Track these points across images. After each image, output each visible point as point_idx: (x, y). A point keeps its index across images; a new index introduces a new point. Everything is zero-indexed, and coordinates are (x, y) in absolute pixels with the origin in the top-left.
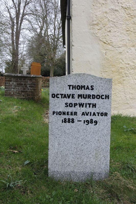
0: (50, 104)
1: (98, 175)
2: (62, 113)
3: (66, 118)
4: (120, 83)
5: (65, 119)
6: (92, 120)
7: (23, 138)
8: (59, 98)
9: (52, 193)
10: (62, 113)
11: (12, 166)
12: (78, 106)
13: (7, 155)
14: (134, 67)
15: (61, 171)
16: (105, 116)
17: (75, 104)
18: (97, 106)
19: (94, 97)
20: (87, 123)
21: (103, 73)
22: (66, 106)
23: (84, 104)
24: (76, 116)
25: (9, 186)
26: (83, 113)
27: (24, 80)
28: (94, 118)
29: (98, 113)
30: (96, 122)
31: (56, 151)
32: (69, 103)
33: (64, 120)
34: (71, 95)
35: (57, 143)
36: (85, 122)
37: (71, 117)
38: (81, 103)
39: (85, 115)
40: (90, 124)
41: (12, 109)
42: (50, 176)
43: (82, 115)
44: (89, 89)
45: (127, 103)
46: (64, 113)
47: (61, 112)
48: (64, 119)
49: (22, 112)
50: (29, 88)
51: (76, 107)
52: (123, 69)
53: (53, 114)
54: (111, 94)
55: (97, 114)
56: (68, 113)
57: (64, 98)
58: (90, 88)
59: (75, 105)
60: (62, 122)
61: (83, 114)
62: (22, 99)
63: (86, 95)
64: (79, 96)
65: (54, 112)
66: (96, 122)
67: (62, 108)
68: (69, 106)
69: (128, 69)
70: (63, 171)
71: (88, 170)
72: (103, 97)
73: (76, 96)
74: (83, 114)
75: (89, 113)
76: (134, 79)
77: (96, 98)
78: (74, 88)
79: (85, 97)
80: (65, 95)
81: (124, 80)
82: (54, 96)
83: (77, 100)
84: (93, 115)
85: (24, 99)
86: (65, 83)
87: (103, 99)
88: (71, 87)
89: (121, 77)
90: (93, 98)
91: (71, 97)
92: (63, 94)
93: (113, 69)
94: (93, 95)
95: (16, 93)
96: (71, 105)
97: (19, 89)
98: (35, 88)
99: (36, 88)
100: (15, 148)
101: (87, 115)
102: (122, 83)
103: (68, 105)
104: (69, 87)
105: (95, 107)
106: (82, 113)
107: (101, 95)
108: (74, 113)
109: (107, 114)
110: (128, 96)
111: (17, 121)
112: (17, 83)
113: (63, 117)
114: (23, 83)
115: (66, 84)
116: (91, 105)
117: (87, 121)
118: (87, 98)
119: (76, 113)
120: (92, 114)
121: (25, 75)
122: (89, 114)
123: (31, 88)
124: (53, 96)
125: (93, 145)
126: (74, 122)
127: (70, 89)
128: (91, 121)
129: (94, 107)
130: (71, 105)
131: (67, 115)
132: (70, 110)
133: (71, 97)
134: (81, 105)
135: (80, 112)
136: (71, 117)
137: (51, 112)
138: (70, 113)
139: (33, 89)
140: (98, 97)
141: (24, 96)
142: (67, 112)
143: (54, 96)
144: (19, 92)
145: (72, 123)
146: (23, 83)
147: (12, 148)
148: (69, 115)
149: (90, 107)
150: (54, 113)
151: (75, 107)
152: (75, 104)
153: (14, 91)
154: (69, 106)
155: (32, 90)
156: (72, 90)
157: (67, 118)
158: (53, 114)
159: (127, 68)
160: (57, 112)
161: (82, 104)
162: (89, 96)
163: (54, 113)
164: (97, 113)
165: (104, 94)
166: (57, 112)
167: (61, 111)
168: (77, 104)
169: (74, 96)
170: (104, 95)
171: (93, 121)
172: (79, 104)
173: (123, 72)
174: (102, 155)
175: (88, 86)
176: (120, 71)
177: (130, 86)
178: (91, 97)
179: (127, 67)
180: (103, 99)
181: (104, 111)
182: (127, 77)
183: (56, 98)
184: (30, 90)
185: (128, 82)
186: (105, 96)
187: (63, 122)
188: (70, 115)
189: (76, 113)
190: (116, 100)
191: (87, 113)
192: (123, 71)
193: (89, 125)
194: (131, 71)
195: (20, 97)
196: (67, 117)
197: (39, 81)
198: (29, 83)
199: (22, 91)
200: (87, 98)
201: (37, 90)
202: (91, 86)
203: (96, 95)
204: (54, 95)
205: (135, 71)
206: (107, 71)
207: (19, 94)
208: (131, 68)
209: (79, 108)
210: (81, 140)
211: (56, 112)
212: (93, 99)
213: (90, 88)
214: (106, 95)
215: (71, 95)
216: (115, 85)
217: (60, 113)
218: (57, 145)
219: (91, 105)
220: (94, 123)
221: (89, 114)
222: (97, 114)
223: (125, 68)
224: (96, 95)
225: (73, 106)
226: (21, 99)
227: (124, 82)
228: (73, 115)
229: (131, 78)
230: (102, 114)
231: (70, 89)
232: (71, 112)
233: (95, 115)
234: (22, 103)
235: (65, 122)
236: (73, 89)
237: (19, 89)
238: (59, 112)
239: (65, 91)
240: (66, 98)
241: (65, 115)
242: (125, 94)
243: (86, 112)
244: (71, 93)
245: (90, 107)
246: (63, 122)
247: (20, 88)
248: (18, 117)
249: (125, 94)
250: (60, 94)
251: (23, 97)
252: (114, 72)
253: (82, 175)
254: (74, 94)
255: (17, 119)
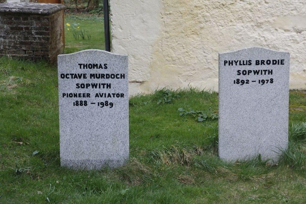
0: (59, 85)
1: (117, 162)
2: (73, 95)
3: (78, 100)
4: (195, 33)
5: (77, 102)
6: (107, 102)
7: (29, 128)
8: (69, 78)
9: (63, 179)
10: (73, 95)
11: (18, 158)
12: (91, 86)
13: (10, 147)
14: (219, 4)
15: (74, 159)
16: (121, 97)
17: (87, 84)
18: (112, 86)
19: (108, 77)
20: (102, 106)
21: (165, 17)
22: (77, 88)
23: (97, 84)
24: (89, 98)
25: (18, 171)
26: (97, 94)
27: (25, 20)
28: (110, 100)
29: (114, 94)
30: (111, 104)
31: (69, 138)
32: (80, 84)
33: (75, 103)
34: (83, 75)
35: (69, 129)
36: (100, 104)
37: (83, 99)
38: (94, 84)
39: (98, 97)
40: (105, 107)
41: (5, 82)
42: (62, 165)
43: (96, 97)
44: (102, 68)
45: (209, 68)
46: (75, 95)
47: (72, 94)
48: (237, 80)
49: (25, 89)
50: (36, 36)
51: (88, 87)
52: (199, 8)
53: (63, 97)
54: (127, 73)
55: (112, 96)
56: (80, 95)
57: (74, 78)
58: (103, 67)
59: (88, 85)
60: (74, 105)
61: (97, 95)
62: (22, 60)
63: (99, 75)
64: (92, 76)
65: (103, 74)
66: (112, 105)
67: (73, 90)
68: (80, 87)
69: (209, 8)
70: (77, 159)
71: (104, 158)
72: (118, 76)
73: (88, 76)
74: (97, 95)
75: (104, 94)
76: (220, 25)
77: (110, 78)
78: (85, 67)
79: (98, 76)
80: (76, 74)
81: (202, 28)
82: (63, 76)
83: (89, 80)
84: (108, 97)
85: (26, 58)
86: (75, 62)
87: (119, 78)
88: (82, 66)
89: (197, 23)
90: (107, 78)
91: (82, 77)
92: (73, 74)
93: (182, 9)
94: (107, 75)
95: (9, 46)
96: (82, 86)
97: (15, 38)
98: (48, 36)
99: (49, 37)
100: (20, 140)
101: (101, 96)
102: (198, 33)
103: (80, 85)
104: (79, 66)
105: (110, 88)
106: (95, 95)
107: (115, 74)
108: (86, 94)
109: (123, 94)
110: (209, 56)
111: (17, 103)
112: (10, 26)
113: (75, 99)
114: (23, 26)
115: (76, 63)
116: (106, 86)
117: (102, 104)
118: (101, 77)
119: (88, 95)
120: (107, 95)
121: (26, 11)
122: (104, 95)
123: (39, 36)
124: (63, 76)
125: (110, 130)
126: (86, 105)
127: (81, 68)
128: (106, 103)
129: (109, 87)
130: (82, 86)
131: (79, 97)
132: (82, 91)
133: (82, 77)
134: (95, 86)
135: (94, 94)
136: (83, 99)
137: (60, 95)
138: (82, 95)
139: (44, 38)
140: (113, 76)
141: (25, 53)
142: (79, 94)
143: (63, 76)
144: (16, 44)
145: (85, 106)
146: (23, 26)
147: (16, 140)
148: (81, 97)
149: (104, 87)
150: (64, 95)
151: (87, 88)
152: (87, 84)
153: (5, 42)
154: (80, 87)
155: (43, 40)
156: (83, 69)
157: (242, 70)
158: (63, 97)
159: (207, 7)
160: (67, 94)
161: (96, 84)
162: (103, 76)
163: (64, 95)
164: (112, 94)
165: (119, 73)
166: (67, 94)
167: (72, 93)
168: (89, 85)
169: (86, 76)
170: (119, 75)
171: (109, 103)
172: (92, 84)
173: (200, 14)
174: (120, 141)
175: (101, 65)
176: (195, 12)
177: (213, 39)
178: (105, 77)
179: (206, 6)
180: (119, 78)
181: (120, 92)
182: (207, 23)
183: (65, 78)
184: (37, 40)
185: (210, 31)
186: (120, 75)
187: (75, 105)
188: (82, 97)
189: (88, 95)
190: (190, 64)
191: (101, 94)
192: (199, 12)
193: (104, 107)
194: (213, 12)
195: (19, 54)
196: (79, 99)
197: (57, 19)
198: (35, 25)
199: (21, 43)
200: (101, 77)
201: (52, 38)
202: (105, 65)
203: (110, 75)
204: (64, 75)
205: (221, 11)
206: (171, 12)
207: (16, 49)
208: (214, 6)
209: (92, 89)
210: (96, 124)
211: (66, 94)
212: (107, 79)
213: (103, 67)
214: (121, 74)
215: (83, 75)
216: (186, 37)
217: (71, 95)
218: (68, 131)
219: (106, 86)
220: (109, 106)
221: (104, 95)
222: (112, 96)
223: (204, 7)
224: (110, 75)
225: (85, 87)
226: (21, 58)
227: (202, 31)
228: (85, 97)
229: (214, 23)
230: (118, 96)
231: (81, 68)
232: (83, 94)
233: (111, 97)
234: (23, 69)
235: (77, 104)
236: (84, 68)
237: (15, 38)
238: (70, 94)
239: (75, 70)
240: (77, 78)
241: (77, 97)
242: (204, 52)
243: (100, 94)
244: (83, 73)
245: (104, 87)
246: (75, 105)
247: (17, 37)
248: (19, 97)
249: (204, 52)
250: (71, 74)
251: (25, 55)
252: (185, 15)
253: (98, 164)
254: (86, 74)
255: (18, 101)
